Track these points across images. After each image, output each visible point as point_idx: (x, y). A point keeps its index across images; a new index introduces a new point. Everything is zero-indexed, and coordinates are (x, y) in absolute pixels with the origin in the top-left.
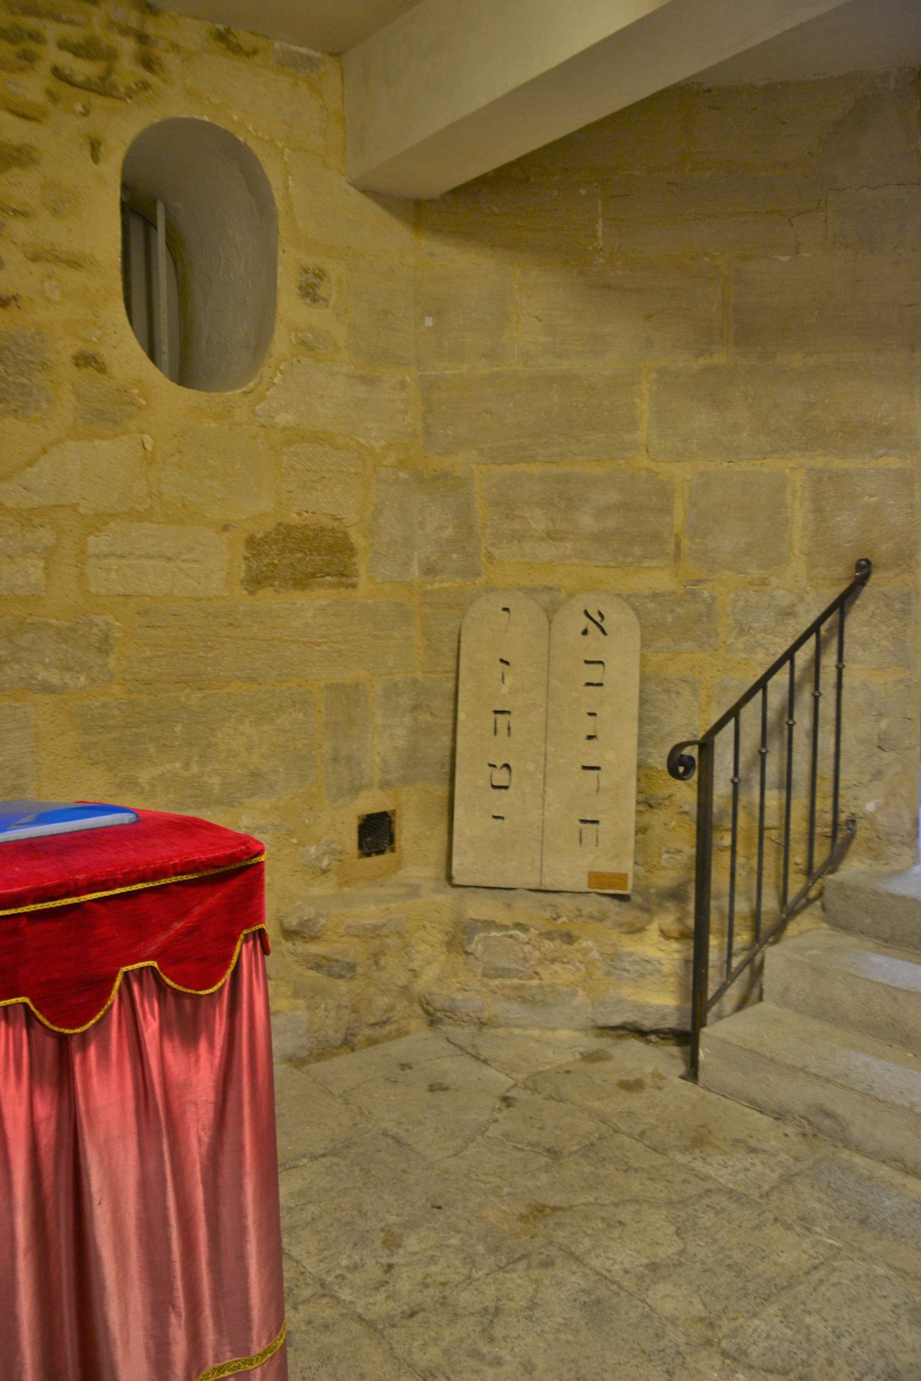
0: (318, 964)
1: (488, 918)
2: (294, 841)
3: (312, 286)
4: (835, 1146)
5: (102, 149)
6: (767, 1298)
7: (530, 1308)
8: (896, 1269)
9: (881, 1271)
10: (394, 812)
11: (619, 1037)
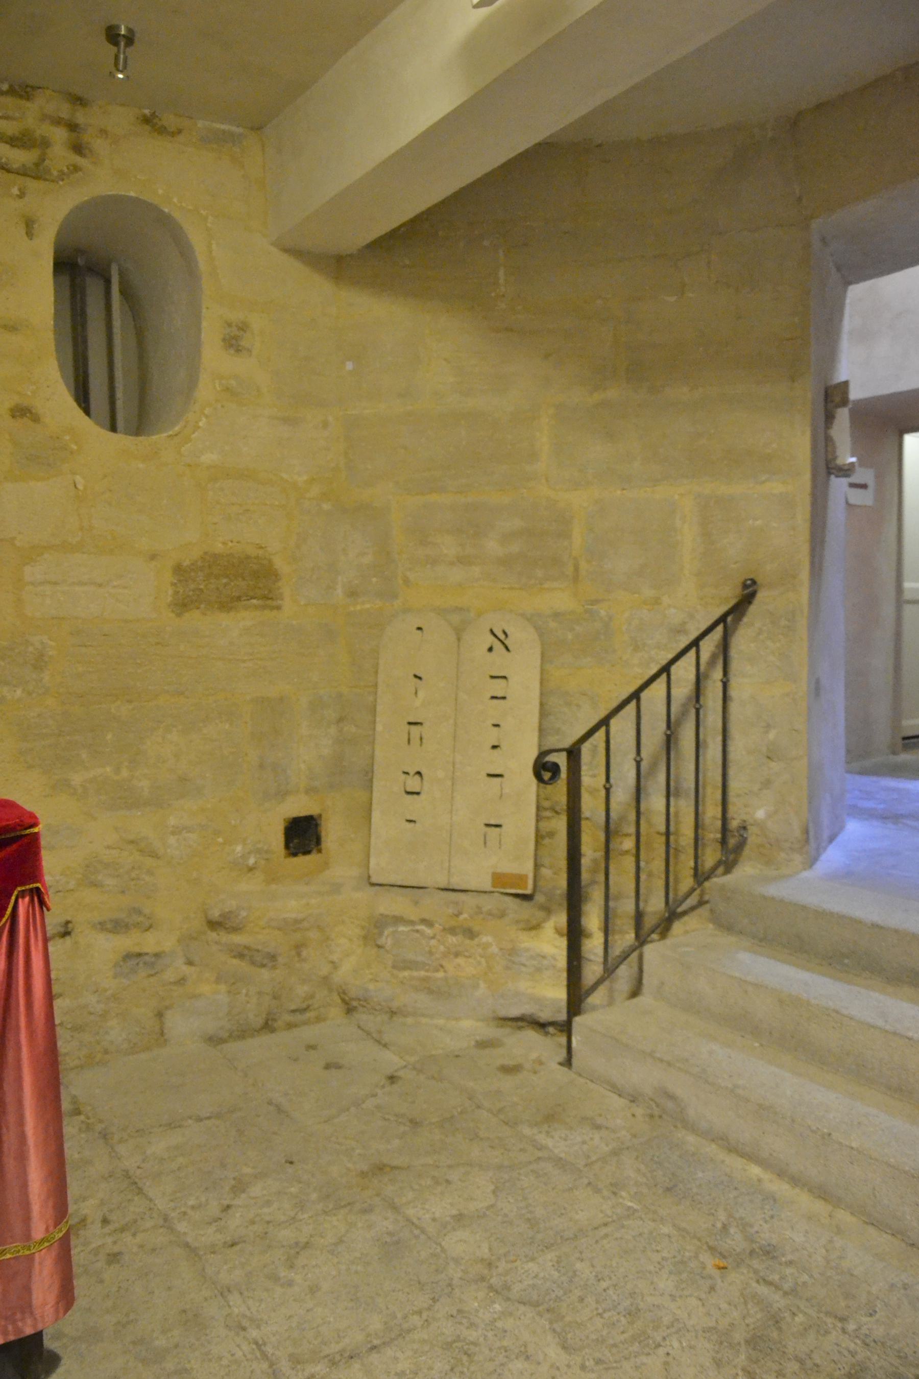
0: (240, 954)
1: (396, 913)
2: (220, 840)
3: (236, 338)
4: (675, 1127)
5: (36, 226)
6: (548, 1247)
7: (336, 1244)
8: (679, 1229)
9: (665, 1230)
10: (320, 816)
11: (520, 1028)
